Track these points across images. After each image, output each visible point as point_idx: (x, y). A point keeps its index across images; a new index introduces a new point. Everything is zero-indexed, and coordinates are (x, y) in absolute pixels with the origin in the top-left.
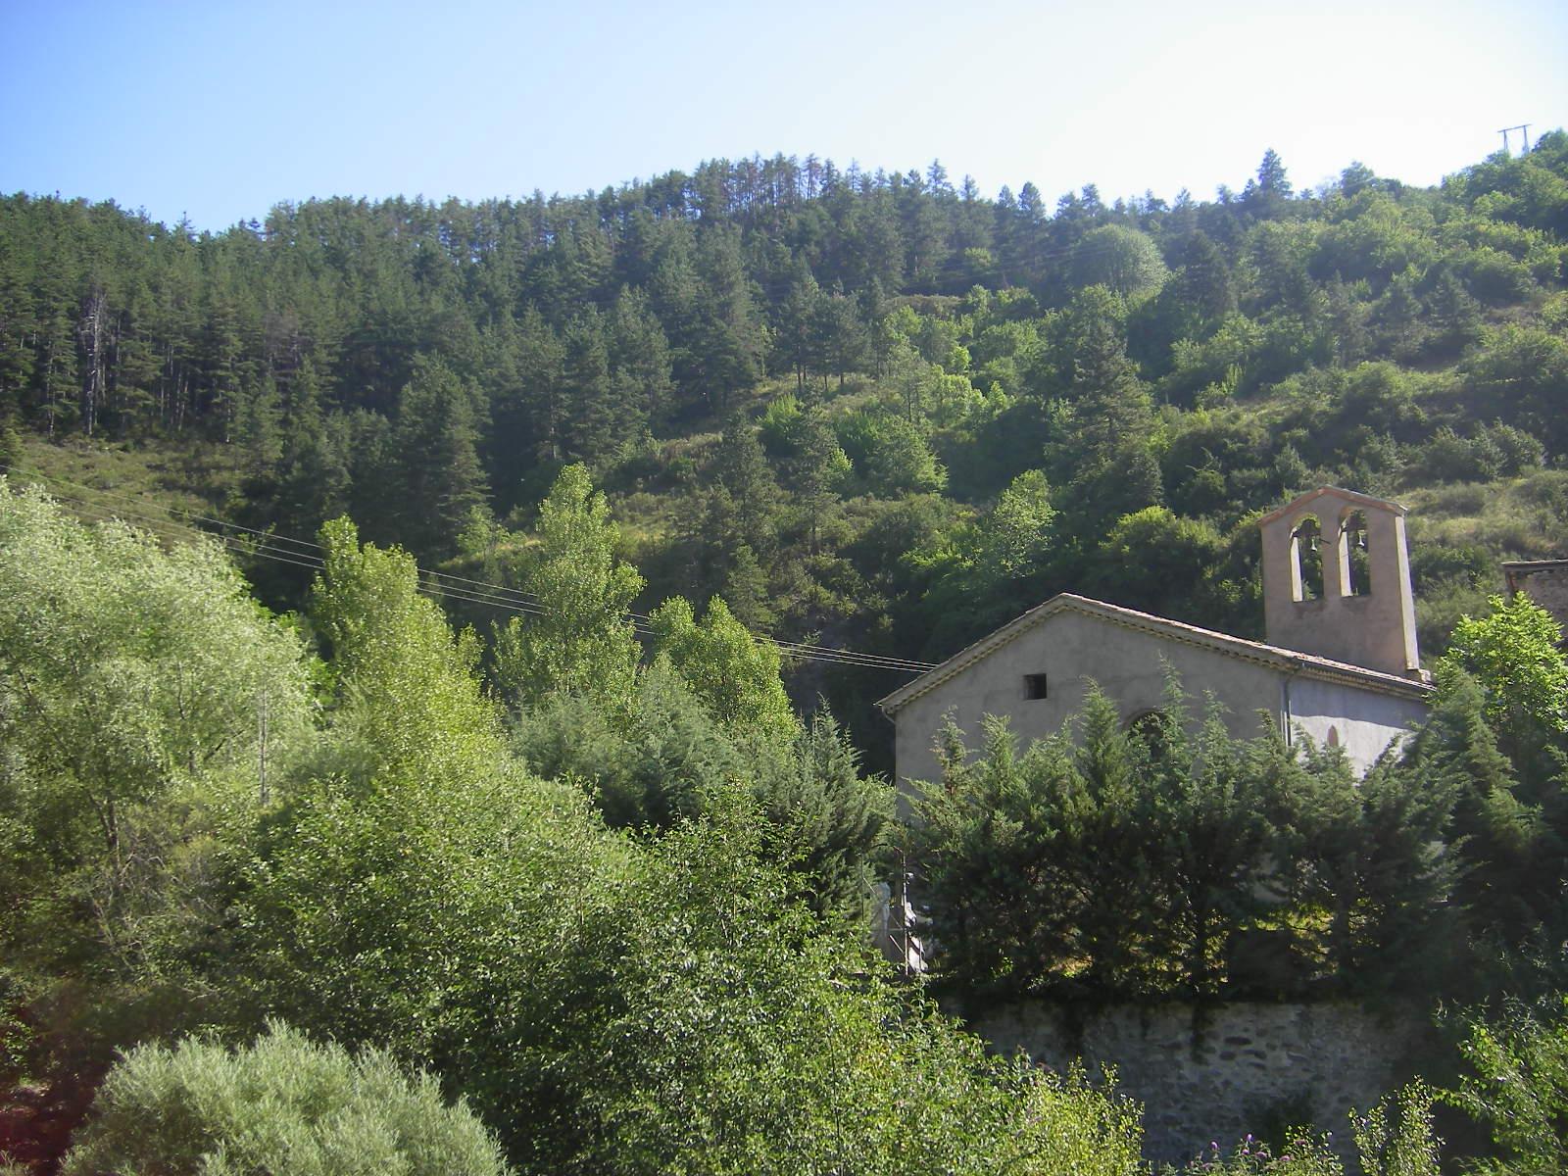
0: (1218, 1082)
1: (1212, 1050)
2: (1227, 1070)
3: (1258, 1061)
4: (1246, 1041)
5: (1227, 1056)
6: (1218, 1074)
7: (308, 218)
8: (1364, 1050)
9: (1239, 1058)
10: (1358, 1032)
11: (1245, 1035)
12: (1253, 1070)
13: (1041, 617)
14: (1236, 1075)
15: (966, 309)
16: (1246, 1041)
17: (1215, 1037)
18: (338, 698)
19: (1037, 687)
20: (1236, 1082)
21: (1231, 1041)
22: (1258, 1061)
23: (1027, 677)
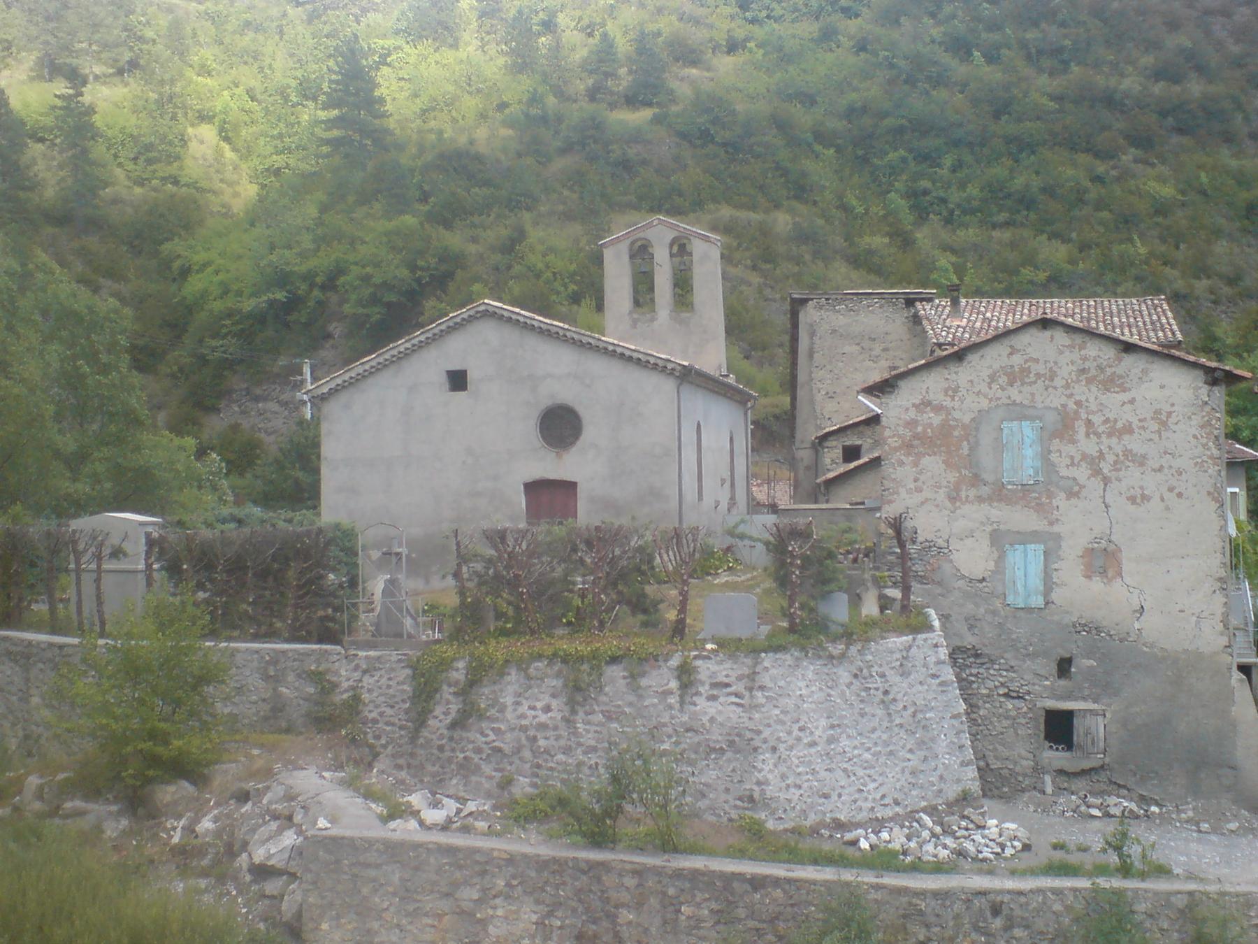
0: (705, 719)
1: (698, 694)
2: (712, 709)
3: (737, 700)
4: (727, 685)
5: (713, 698)
6: (706, 713)
7: (318, 535)
8: (814, 688)
9: (722, 699)
10: (810, 675)
11: (726, 680)
12: (734, 708)
13: (463, 319)
14: (720, 712)
15: (660, 882)
16: (727, 685)
17: (703, 683)
18: (149, 591)
19: (458, 380)
20: (720, 719)
21: (715, 685)
22: (737, 700)
23: (449, 373)
